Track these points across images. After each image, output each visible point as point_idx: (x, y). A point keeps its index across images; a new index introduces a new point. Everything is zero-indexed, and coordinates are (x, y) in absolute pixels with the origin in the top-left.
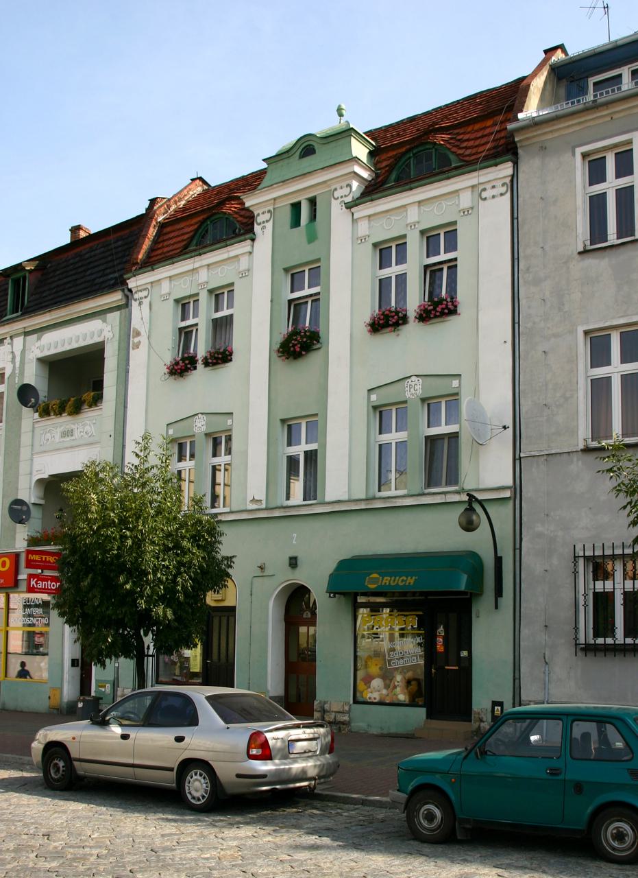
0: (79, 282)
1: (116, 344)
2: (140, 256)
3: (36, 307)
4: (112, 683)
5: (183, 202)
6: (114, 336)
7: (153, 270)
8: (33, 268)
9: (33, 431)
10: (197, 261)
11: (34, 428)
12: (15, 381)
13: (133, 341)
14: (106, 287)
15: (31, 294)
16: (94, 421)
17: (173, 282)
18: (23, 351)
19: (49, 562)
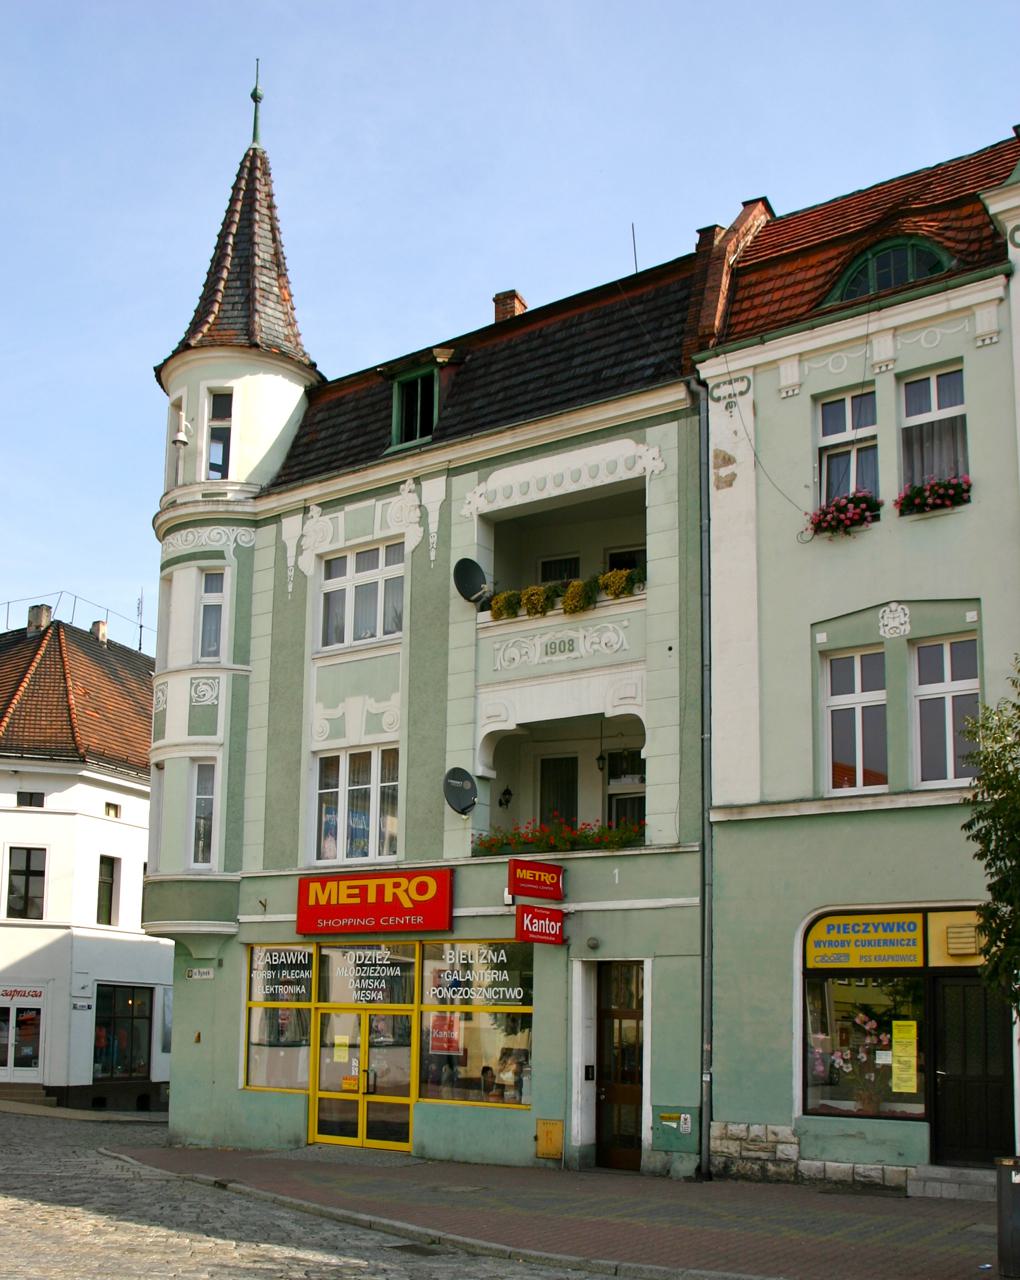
0: (556, 378)
1: (673, 483)
2: (717, 323)
3: (462, 427)
4: (697, 1112)
5: (750, 238)
6: (665, 468)
7: (763, 342)
8: (446, 360)
9: (476, 645)
10: (875, 321)
11: (477, 639)
12: (429, 557)
13: (717, 475)
14: (638, 381)
15: (443, 408)
16: (625, 623)
17: (898, 338)
18: (446, 507)
19: (544, 882)
